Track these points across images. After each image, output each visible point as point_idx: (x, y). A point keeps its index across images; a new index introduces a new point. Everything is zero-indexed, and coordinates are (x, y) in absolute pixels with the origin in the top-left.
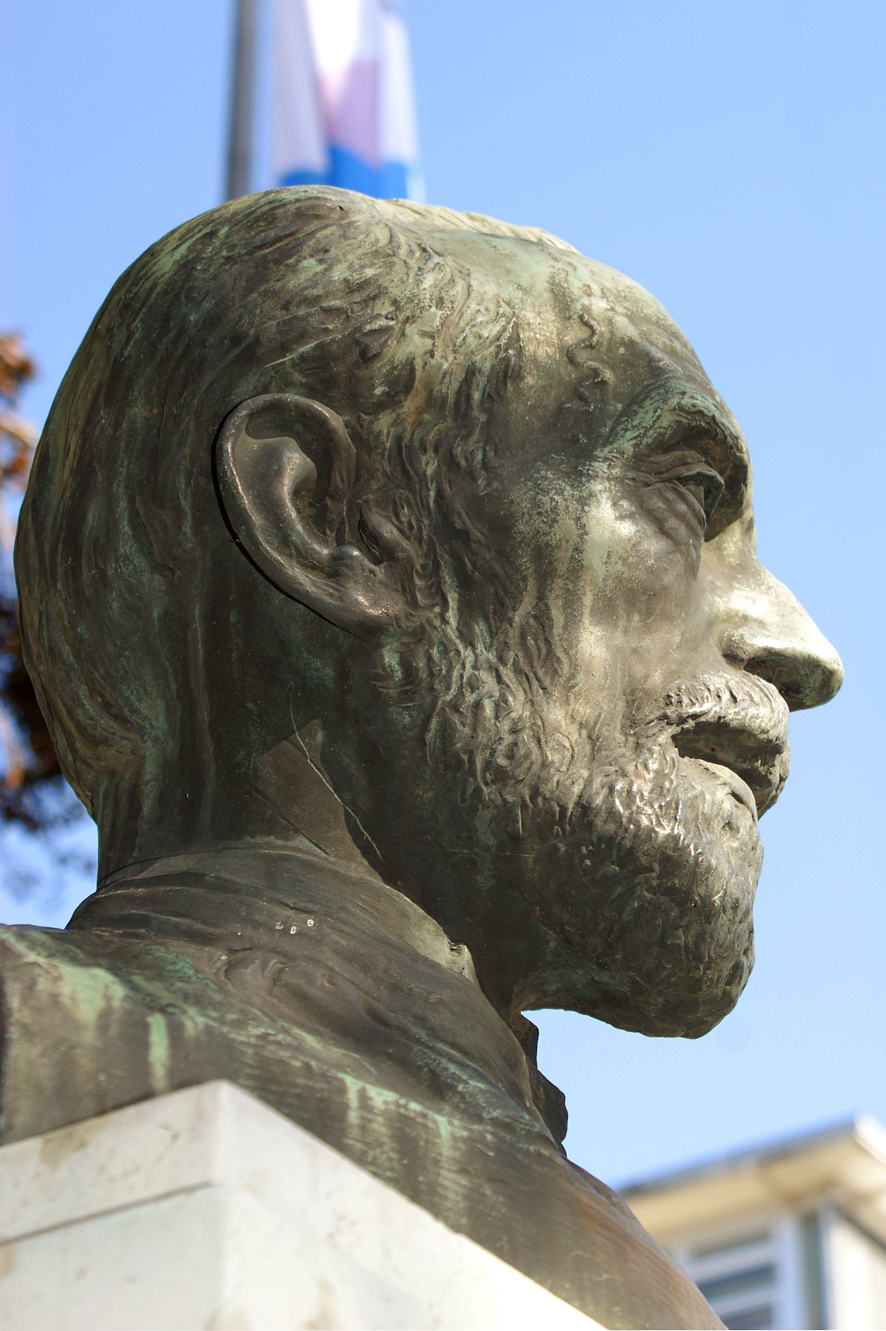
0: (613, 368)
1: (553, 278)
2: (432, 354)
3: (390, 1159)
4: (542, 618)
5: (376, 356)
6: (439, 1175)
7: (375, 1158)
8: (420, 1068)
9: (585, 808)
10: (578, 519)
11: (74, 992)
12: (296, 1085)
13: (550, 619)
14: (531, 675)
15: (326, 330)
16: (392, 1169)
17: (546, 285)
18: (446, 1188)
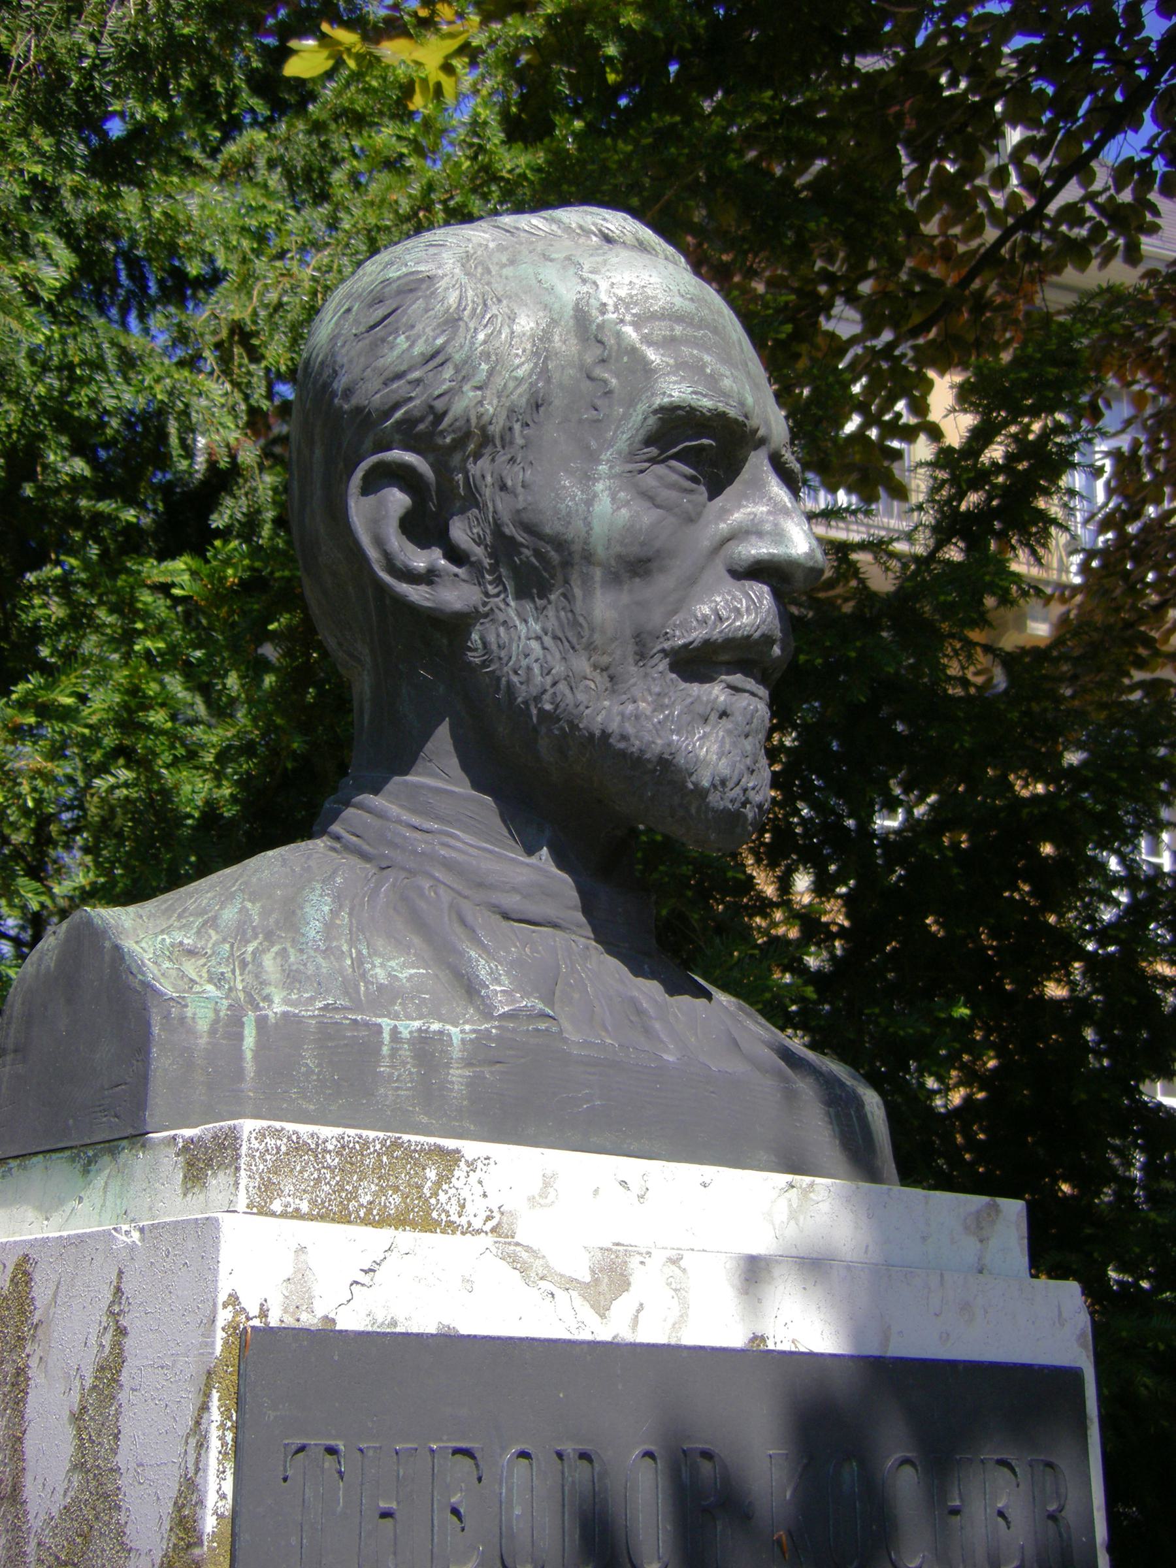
0: (617, 377)
1: (577, 304)
2: (481, 403)
3: (411, 1073)
5: (445, 413)
6: (449, 1074)
7: (399, 1075)
8: (463, 976)
9: (605, 735)
10: (586, 518)
11: (195, 1014)
12: (345, 1037)
13: (574, 596)
14: (564, 639)
15: (411, 399)
16: (411, 1081)
17: (572, 313)
18: (452, 1083)
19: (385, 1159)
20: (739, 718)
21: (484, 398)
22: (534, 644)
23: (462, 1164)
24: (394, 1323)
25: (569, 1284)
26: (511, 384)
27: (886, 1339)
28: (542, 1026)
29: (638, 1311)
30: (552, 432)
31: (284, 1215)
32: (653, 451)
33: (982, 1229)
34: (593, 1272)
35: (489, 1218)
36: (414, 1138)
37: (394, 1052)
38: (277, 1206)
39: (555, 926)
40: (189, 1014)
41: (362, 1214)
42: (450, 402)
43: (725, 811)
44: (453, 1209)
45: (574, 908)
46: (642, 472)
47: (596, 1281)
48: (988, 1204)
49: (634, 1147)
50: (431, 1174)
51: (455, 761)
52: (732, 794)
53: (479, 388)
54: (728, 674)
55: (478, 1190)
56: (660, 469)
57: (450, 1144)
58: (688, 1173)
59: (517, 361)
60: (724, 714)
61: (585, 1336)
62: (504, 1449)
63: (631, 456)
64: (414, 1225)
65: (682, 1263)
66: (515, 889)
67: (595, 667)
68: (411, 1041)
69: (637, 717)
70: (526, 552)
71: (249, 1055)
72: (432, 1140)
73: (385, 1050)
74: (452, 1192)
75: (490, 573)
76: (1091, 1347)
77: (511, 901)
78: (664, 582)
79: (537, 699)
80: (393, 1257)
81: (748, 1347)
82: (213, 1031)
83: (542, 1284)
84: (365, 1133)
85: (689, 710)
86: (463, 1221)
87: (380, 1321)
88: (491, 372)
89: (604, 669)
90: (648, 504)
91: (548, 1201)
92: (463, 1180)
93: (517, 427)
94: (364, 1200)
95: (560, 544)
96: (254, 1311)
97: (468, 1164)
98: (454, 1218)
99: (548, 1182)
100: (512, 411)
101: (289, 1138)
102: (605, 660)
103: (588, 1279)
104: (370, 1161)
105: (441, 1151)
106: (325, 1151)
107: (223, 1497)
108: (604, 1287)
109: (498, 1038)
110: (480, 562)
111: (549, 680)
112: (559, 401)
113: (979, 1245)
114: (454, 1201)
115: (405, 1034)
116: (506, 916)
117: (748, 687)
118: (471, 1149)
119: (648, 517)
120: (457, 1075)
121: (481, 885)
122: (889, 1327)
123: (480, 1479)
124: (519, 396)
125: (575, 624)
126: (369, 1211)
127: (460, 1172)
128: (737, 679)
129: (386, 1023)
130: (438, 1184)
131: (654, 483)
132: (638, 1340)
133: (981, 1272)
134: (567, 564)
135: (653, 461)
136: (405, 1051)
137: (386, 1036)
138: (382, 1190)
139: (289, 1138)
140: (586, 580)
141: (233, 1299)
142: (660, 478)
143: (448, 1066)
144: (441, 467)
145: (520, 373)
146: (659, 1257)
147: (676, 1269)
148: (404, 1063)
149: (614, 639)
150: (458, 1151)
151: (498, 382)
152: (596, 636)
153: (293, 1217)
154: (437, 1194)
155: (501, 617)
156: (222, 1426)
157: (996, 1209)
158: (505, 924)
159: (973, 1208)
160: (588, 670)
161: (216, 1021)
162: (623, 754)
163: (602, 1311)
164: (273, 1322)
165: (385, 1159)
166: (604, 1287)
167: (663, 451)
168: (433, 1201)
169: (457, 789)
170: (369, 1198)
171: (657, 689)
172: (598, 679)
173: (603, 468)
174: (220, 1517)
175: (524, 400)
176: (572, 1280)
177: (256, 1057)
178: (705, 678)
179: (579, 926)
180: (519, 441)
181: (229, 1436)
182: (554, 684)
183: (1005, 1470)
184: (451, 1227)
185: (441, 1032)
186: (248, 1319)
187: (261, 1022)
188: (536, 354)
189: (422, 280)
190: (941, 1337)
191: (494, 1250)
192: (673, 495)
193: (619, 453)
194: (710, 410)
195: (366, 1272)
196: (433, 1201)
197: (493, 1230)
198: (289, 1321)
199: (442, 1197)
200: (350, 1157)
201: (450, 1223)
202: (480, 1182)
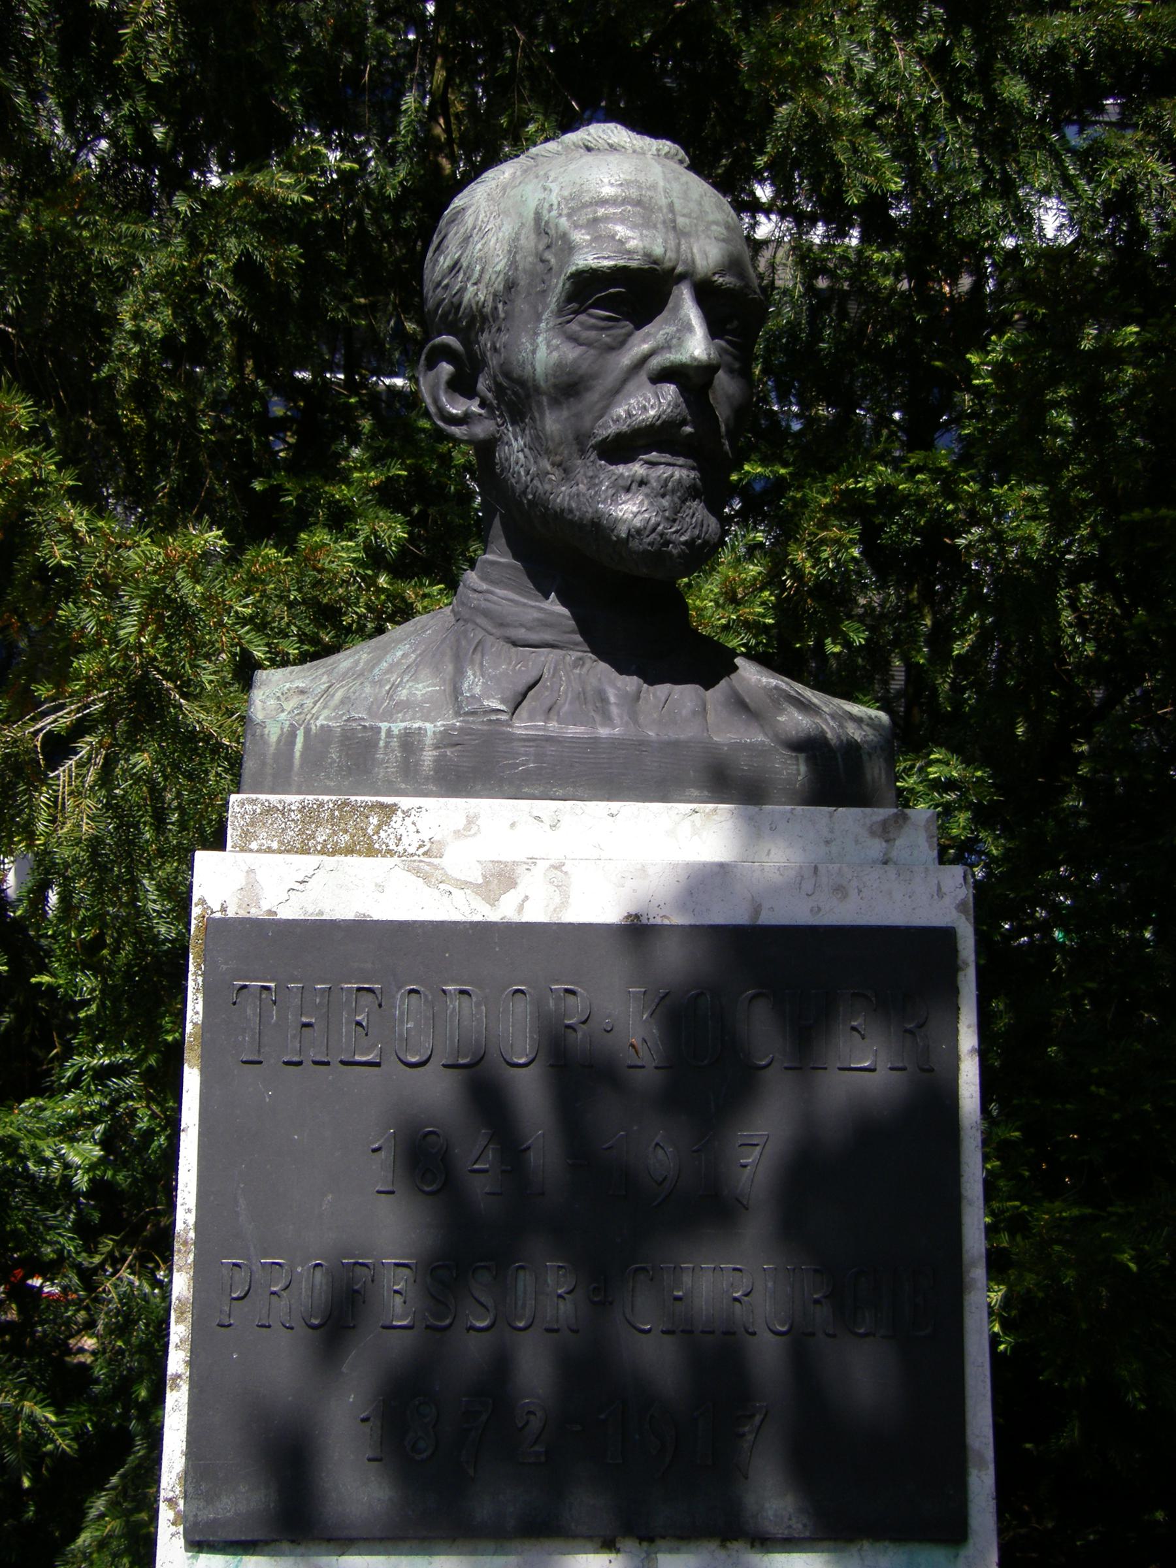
4: (533, 419)
5: (460, 305)
19: (337, 813)
21: (478, 290)
22: (521, 455)
23: (399, 813)
24: (321, 913)
25: (464, 885)
26: (494, 277)
28: (494, 717)
29: (524, 901)
30: (522, 305)
31: (259, 851)
32: (574, 306)
34: (484, 877)
35: (420, 846)
36: (359, 798)
37: (387, 744)
38: (254, 845)
40: (266, 732)
41: (319, 848)
42: (461, 298)
43: (645, 552)
45: (572, 632)
46: (569, 322)
47: (487, 883)
48: (895, 814)
50: (374, 820)
51: (503, 541)
52: (648, 540)
53: (475, 284)
54: (645, 454)
55: (412, 828)
56: (582, 317)
58: (598, 809)
59: (497, 260)
61: (477, 918)
62: (400, 988)
63: (560, 312)
64: (360, 853)
65: (563, 868)
66: (522, 625)
67: (553, 464)
68: (399, 736)
69: (578, 495)
70: (509, 392)
71: (297, 754)
72: (374, 799)
73: (382, 744)
74: (389, 831)
75: (498, 409)
76: (971, 912)
77: (521, 634)
78: (592, 397)
79: (524, 493)
80: (320, 873)
82: (279, 741)
83: (441, 886)
84: (321, 798)
85: (614, 485)
86: (400, 849)
87: (311, 911)
88: (482, 271)
89: (559, 465)
90: (572, 345)
91: (473, 832)
92: (399, 823)
93: (500, 306)
94: (320, 840)
95: (521, 382)
96: (216, 907)
97: (403, 812)
99: (471, 820)
100: (495, 295)
101: (263, 804)
102: (558, 458)
103: (480, 881)
104: (325, 815)
105: (382, 806)
106: (290, 810)
107: (197, 1013)
108: (494, 886)
109: (461, 729)
110: (491, 403)
111: (529, 478)
112: (523, 281)
113: (884, 844)
114: (392, 836)
115: (396, 732)
116: (515, 644)
117: (663, 460)
118: (405, 802)
119: (571, 353)
120: (428, 756)
121: (502, 625)
122: (760, 906)
123: (380, 1006)
124: (499, 285)
125: (538, 437)
126: (324, 846)
127: (397, 818)
129: (384, 726)
130: (379, 827)
131: (578, 328)
132: (524, 920)
133: (885, 863)
134: (528, 396)
135: (577, 312)
136: (395, 743)
137: (383, 734)
138: (335, 833)
139: (263, 804)
140: (540, 404)
141: (202, 901)
142: (581, 324)
143: (422, 750)
144: (467, 342)
145: (498, 268)
146: (542, 866)
147: (559, 873)
148: (393, 751)
149: (560, 444)
150: (395, 805)
151: (486, 277)
152: (550, 443)
153: (265, 852)
154: (378, 833)
155: (505, 439)
156: (195, 974)
158: (514, 649)
159: (881, 818)
160: (549, 468)
161: (281, 735)
162: (572, 522)
163: (493, 902)
164: (231, 913)
165: (337, 813)
166: (494, 886)
167: (582, 304)
168: (375, 837)
169: (502, 560)
170: (324, 837)
171: (590, 474)
172: (557, 473)
173: (543, 325)
174: (195, 1024)
175: (502, 286)
176: (466, 883)
177: (302, 754)
178: (628, 459)
179: (577, 644)
180: (502, 315)
181: (200, 979)
182: (532, 480)
184: (390, 853)
185: (420, 728)
186: (212, 912)
187: (307, 731)
188: (510, 252)
189: (459, 212)
190: (811, 911)
191: (401, 865)
192: (593, 334)
193: (552, 312)
194: (609, 268)
195: (301, 882)
196: (375, 837)
198: (243, 914)
199: (383, 834)
200: (310, 815)
202: (414, 823)
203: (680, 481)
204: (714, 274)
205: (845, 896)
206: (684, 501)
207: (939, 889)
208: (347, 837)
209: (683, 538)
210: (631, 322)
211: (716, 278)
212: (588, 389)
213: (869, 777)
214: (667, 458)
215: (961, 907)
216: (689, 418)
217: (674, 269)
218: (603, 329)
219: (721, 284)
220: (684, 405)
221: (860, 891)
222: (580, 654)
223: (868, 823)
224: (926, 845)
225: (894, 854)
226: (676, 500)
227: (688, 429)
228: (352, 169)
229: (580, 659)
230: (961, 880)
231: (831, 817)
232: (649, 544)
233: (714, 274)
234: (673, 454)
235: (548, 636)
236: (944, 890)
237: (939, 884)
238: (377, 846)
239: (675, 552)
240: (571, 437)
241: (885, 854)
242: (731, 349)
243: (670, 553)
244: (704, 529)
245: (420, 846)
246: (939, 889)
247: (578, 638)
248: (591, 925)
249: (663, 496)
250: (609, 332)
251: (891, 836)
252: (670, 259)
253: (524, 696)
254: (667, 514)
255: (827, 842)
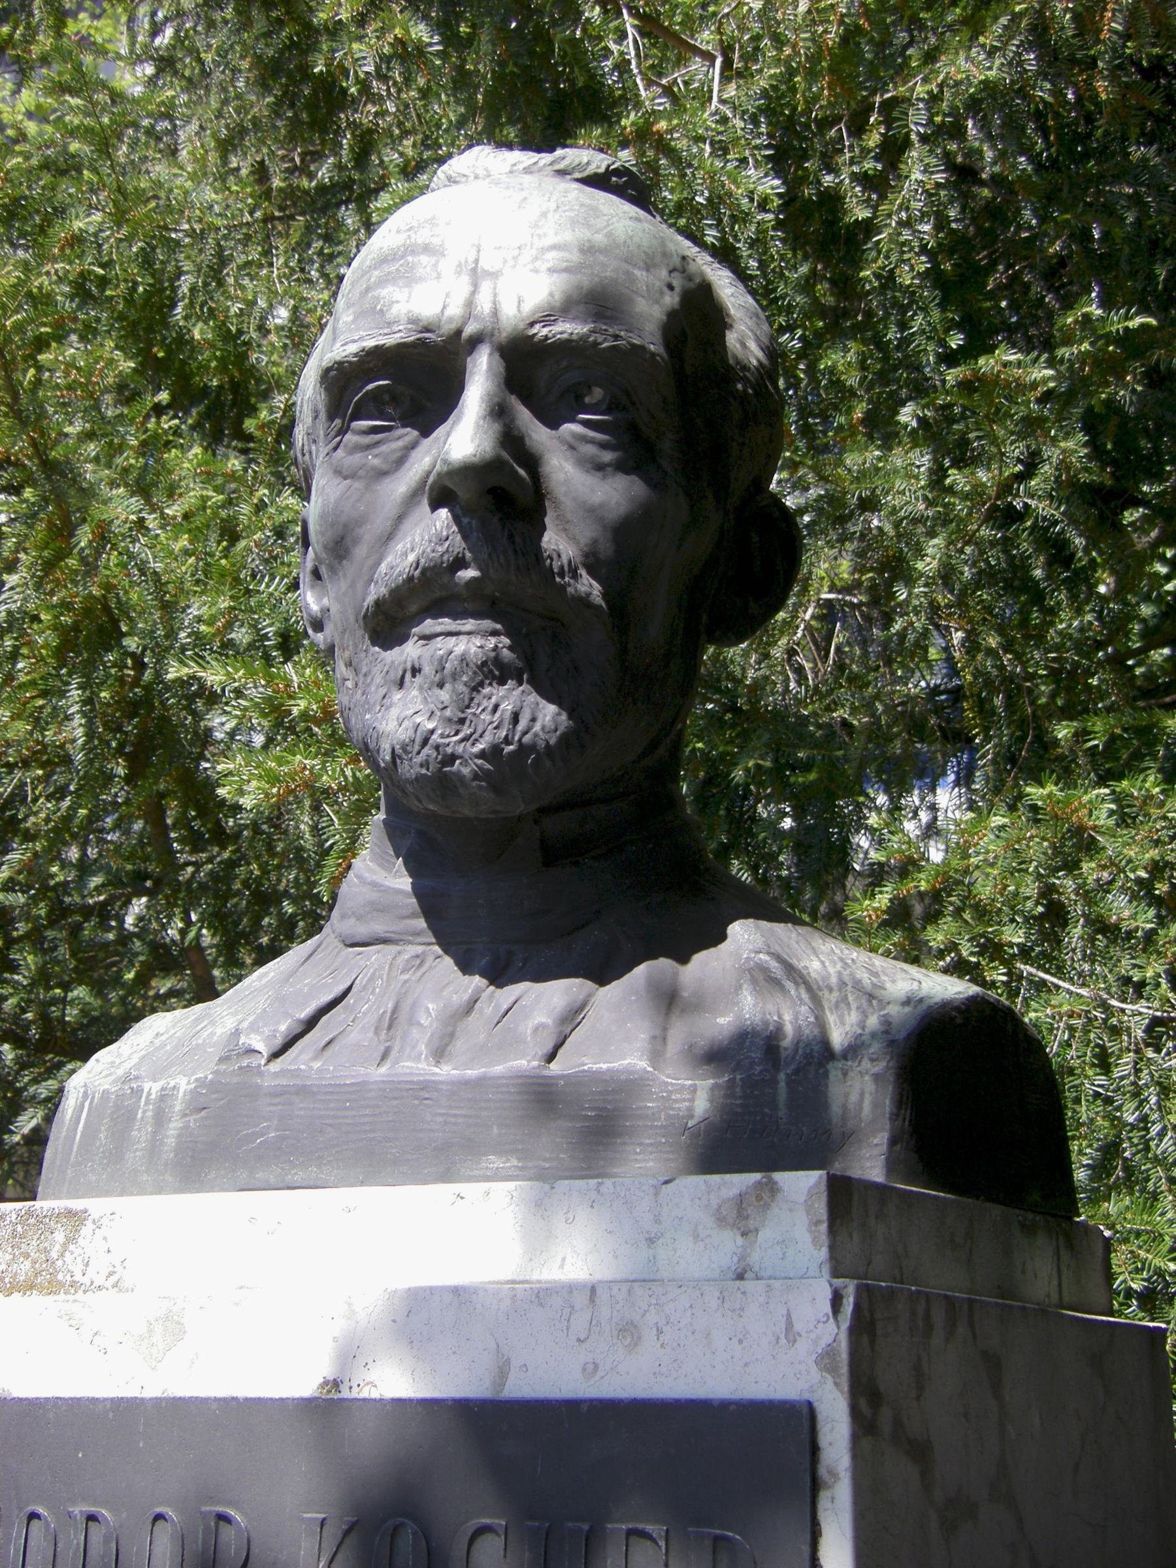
19: (19, 1228)
20: (428, 669)
23: (89, 1223)
27: (502, 1373)
32: (338, 422)
33: (747, 1217)
35: (111, 1274)
39: (385, 941)
43: (419, 778)
44: (77, 1269)
45: (413, 916)
48: (759, 1183)
49: (298, 1176)
52: (418, 759)
57: (76, 1204)
60: (415, 671)
73: (139, 1115)
76: (844, 1370)
78: (360, 552)
81: (317, 1395)
86: (86, 1280)
98: (78, 1277)
105: (70, 1213)
113: (740, 1241)
114: (79, 1259)
117: (439, 629)
118: (95, 1206)
122: (508, 1362)
127: (87, 1230)
128: (429, 625)
130: (65, 1247)
133: (740, 1277)
157: (773, 1189)
159: (735, 1191)
165: (19, 1228)
179: (418, 934)
183: (649, 1543)
190: (584, 1369)
194: (356, 355)
197: (115, 1285)
199: (68, 1257)
201: (73, 1284)
202: (105, 1238)
203: (463, 659)
204: (532, 324)
205: (636, 1342)
206: (476, 688)
207: (789, 1325)
208: (28, 1263)
209: (480, 746)
210: (414, 427)
211: (534, 331)
212: (356, 541)
213: (836, 1109)
214: (446, 624)
215: (826, 1360)
216: (468, 555)
217: (459, 332)
218: (368, 447)
219: (546, 338)
220: (459, 537)
221: (660, 1332)
222: (420, 949)
223: (714, 1202)
224: (808, 1238)
225: (755, 1258)
226: (461, 688)
227: (470, 573)
228: (1144, 327)
229: (417, 956)
230: (827, 1308)
231: (656, 1194)
232: (421, 766)
233: (532, 324)
234: (455, 616)
235: (378, 927)
236: (798, 1326)
237: (789, 1315)
238: (60, 1277)
239: (466, 771)
240: (352, 618)
241: (742, 1258)
242: (592, 434)
243: (458, 774)
244: (521, 727)
245: (111, 1274)
246: (789, 1325)
247: (421, 923)
248: (259, 1400)
249: (441, 685)
250: (376, 451)
251: (752, 1223)
252: (451, 320)
253: (311, 1023)
254: (448, 713)
255: (651, 1241)
